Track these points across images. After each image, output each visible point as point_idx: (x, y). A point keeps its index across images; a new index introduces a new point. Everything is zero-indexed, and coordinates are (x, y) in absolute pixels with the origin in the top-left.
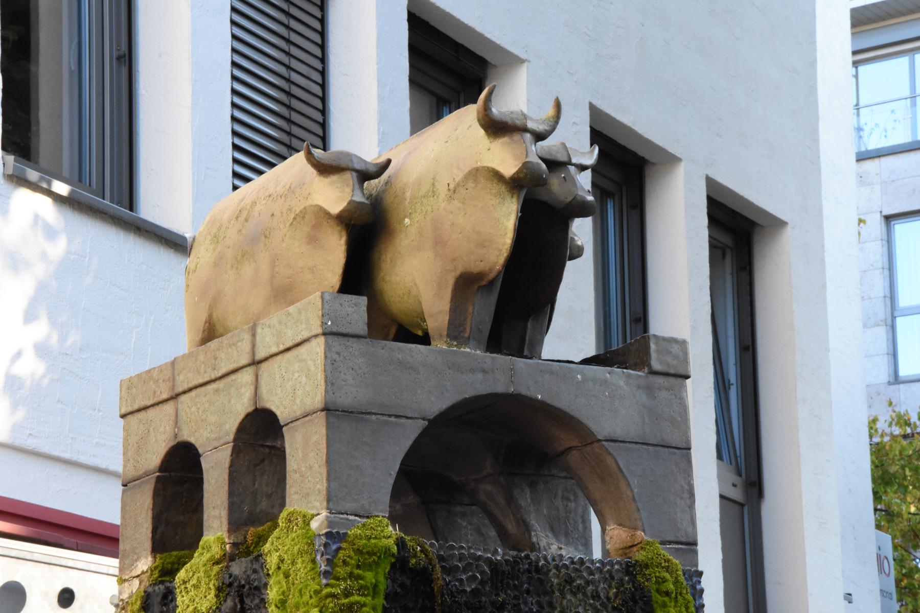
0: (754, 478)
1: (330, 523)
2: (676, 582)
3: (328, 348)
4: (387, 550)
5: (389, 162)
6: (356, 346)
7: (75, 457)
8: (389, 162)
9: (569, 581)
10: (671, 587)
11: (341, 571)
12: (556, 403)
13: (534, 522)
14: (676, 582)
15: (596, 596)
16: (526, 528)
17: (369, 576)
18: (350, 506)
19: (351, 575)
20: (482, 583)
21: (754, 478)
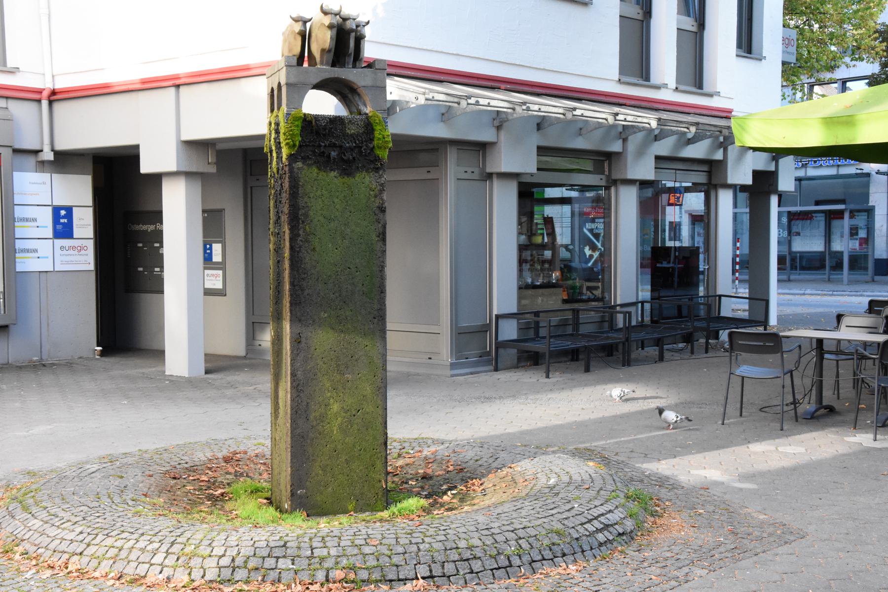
0: (702, 23)
1: (287, 111)
2: (379, 120)
3: (287, 69)
4: (301, 117)
5: (312, 18)
6: (294, 68)
7: (398, 44)
8: (312, 18)
9: (350, 121)
10: (377, 121)
11: (289, 122)
12: (348, 79)
13: (360, 104)
14: (379, 120)
15: (358, 125)
16: (358, 105)
17: (296, 123)
18: (292, 107)
19: (292, 123)
20: (327, 123)
21: (702, 23)
